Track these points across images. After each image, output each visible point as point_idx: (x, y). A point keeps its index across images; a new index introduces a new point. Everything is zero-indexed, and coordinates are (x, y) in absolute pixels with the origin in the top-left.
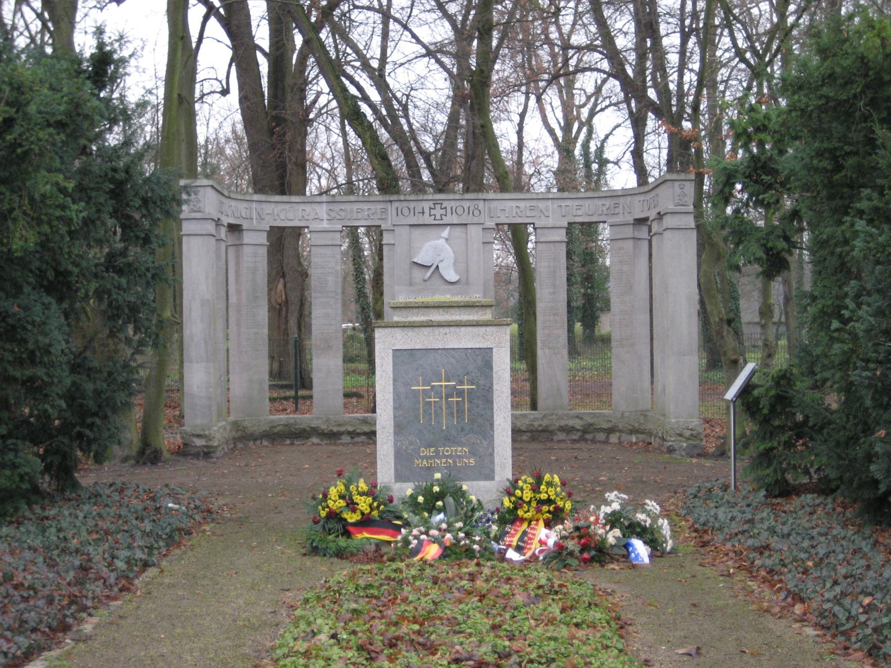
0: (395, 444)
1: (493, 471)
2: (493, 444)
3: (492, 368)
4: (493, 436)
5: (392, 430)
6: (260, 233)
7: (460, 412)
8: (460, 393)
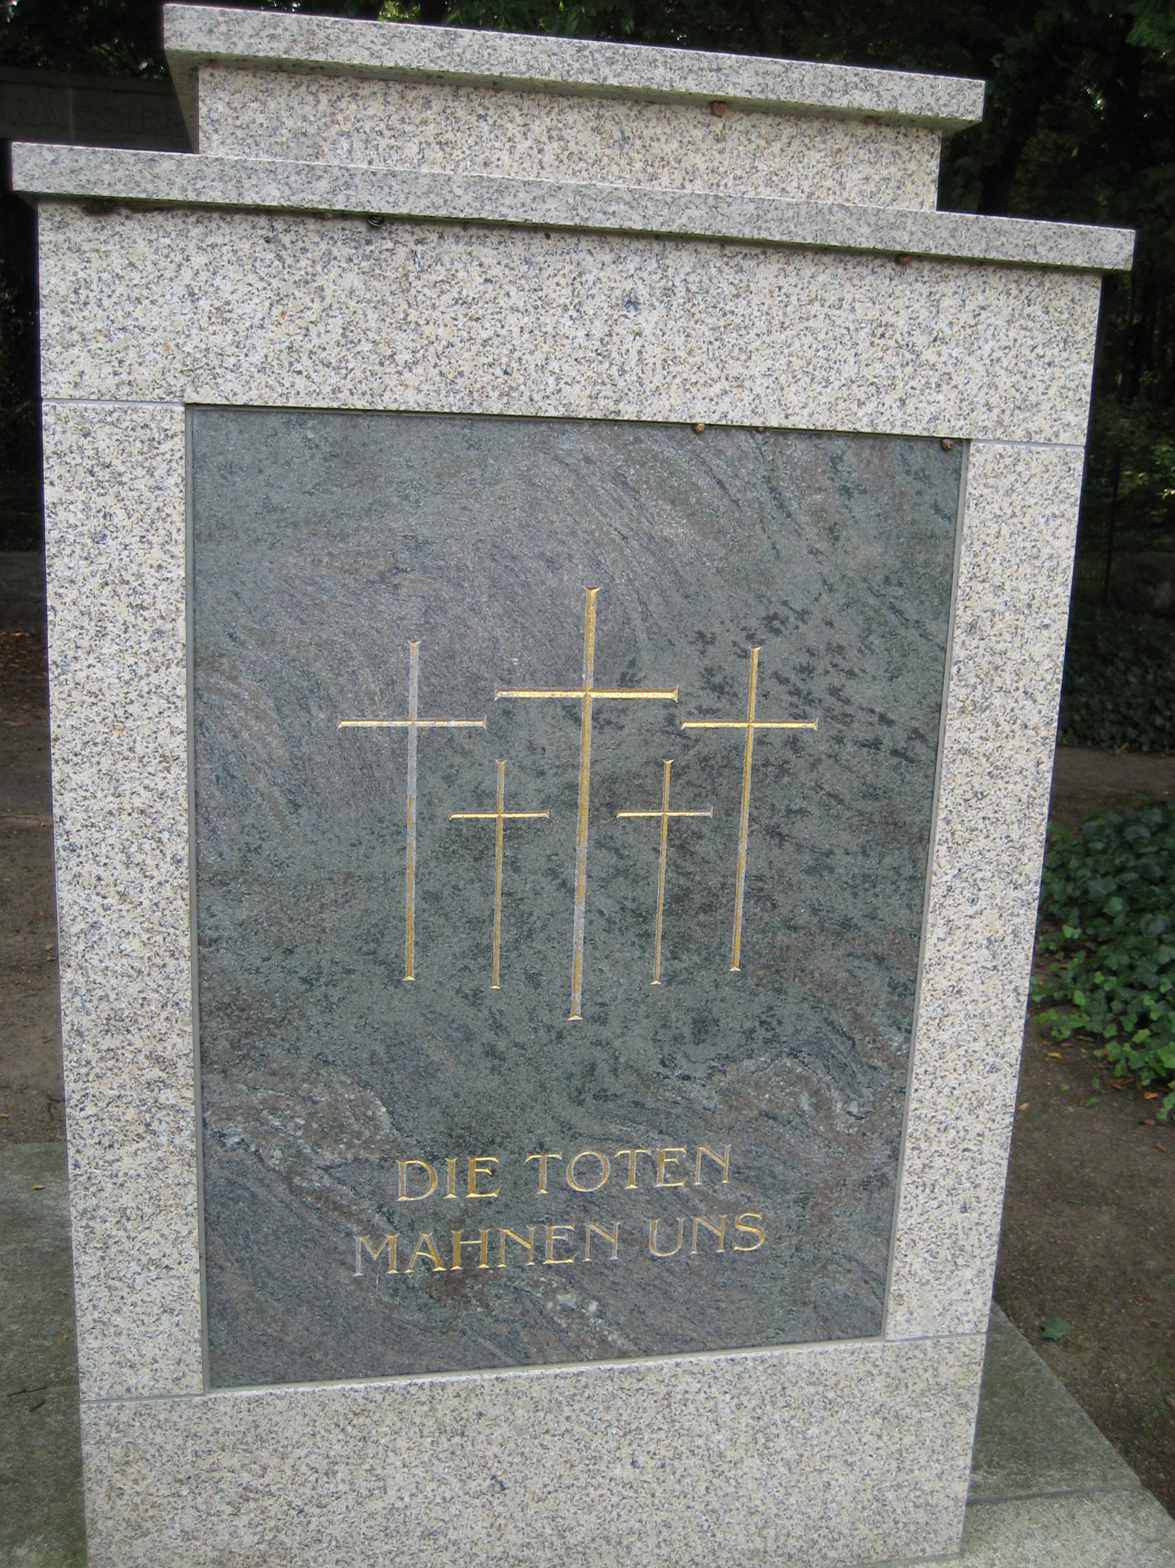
0: (210, 1138)
1: (877, 1281)
2: (898, 1117)
3: (945, 593)
4: (901, 1064)
5: (181, 1044)
6: (1072, 285)
7: (696, 902)
8: (710, 769)
